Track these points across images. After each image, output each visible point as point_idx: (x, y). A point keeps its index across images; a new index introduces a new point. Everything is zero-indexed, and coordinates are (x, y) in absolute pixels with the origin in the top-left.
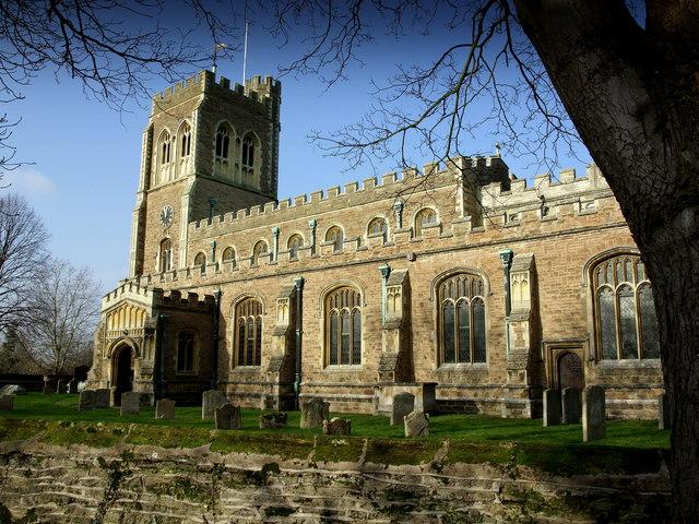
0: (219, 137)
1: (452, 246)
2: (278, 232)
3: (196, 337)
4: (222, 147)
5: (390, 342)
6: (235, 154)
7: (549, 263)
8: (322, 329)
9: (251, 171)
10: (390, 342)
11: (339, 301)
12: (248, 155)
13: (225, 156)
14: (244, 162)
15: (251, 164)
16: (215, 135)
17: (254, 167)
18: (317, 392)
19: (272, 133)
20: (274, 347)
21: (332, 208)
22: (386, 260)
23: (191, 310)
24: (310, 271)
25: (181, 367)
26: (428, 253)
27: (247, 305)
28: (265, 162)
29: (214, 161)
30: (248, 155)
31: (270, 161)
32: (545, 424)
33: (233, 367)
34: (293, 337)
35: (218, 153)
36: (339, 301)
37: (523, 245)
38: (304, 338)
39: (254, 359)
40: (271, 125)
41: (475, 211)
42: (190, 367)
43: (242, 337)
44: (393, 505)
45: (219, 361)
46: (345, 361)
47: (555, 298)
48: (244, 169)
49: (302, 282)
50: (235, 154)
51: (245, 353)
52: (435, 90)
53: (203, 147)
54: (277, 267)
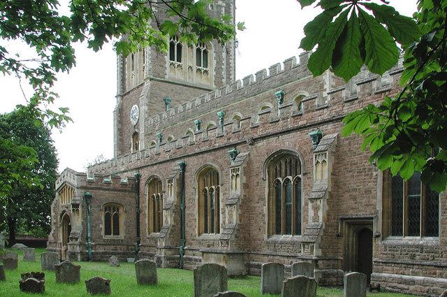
0: (172, 45)
1: (280, 129)
2: (199, 124)
3: (121, 210)
5: (231, 216)
6: (189, 57)
7: (350, 144)
8: (197, 205)
9: (206, 72)
10: (231, 216)
11: (283, 171)
12: (202, 56)
13: (179, 60)
14: (199, 64)
15: (206, 66)
18: (194, 255)
20: (168, 219)
21: (234, 101)
22: (235, 145)
23: (114, 190)
24: (189, 156)
26: (263, 138)
27: (154, 182)
28: (219, 62)
29: (167, 65)
30: (202, 56)
33: (149, 234)
34: (245, 205)
35: (172, 58)
36: (283, 171)
37: (330, 126)
38: (187, 212)
39: (157, 228)
42: (117, 233)
43: (278, 201)
45: (187, 229)
46: (287, 232)
47: (352, 176)
48: (199, 70)
49: (184, 166)
50: (189, 57)
51: (157, 224)
52: (73, 65)
54: (170, 153)
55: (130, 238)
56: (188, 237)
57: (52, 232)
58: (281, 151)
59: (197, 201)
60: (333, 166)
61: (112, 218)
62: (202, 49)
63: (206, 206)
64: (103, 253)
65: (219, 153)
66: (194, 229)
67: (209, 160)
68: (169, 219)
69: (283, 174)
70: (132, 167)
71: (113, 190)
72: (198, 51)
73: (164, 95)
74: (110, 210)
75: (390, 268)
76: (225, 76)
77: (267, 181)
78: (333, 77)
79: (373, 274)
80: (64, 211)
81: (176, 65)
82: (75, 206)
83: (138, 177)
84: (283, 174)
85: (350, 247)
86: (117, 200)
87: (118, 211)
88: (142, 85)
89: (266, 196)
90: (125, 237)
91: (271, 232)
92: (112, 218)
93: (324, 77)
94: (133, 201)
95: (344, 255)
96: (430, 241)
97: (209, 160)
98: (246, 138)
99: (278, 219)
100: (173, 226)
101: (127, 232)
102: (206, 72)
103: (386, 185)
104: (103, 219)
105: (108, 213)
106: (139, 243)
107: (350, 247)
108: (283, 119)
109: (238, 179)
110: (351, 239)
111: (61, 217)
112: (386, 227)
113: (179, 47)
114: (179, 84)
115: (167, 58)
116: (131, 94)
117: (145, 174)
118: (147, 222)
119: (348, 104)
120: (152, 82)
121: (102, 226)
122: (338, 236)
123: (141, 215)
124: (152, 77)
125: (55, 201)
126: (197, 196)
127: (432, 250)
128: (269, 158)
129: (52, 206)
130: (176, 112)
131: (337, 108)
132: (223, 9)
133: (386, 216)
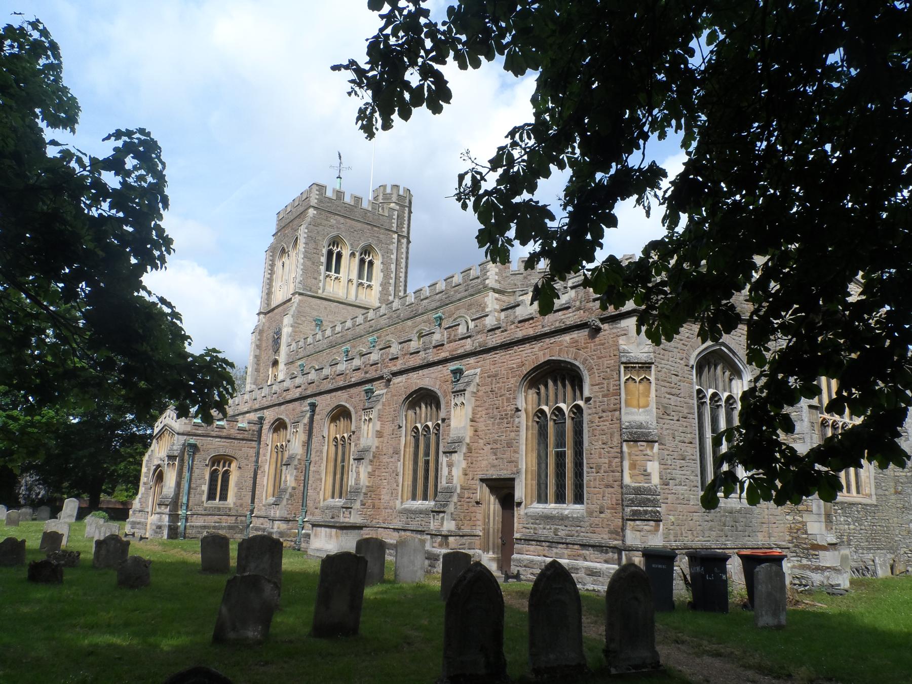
0: (330, 253)
3: (233, 465)
4: (333, 261)
6: (349, 267)
8: (325, 459)
9: (369, 286)
13: (337, 271)
14: (360, 276)
15: (369, 278)
16: (325, 251)
17: (372, 283)
19: (395, 245)
25: (211, 496)
28: (387, 276)
29: (322, 278)
30: (365, 266)
31: (393, 275)
32: (165, 537)
35: (328, 268)
37: (472, 360)
39: (543, 495)
40: (395, 236)
41: (709, 502)
42: (224, 497)
44: (632, 510)
49: (313, 406)
50: (349, 267)
53: (309, 263)
55: (241, 505)
56: (310, 503)
57: (139, 496)
58: (421, 389)
59: (325, 455)
60: (473, 410)
61: (220, 477)
62: (367, 259)
63: (336, 460)
64: (201, 527)
65: (353, 391)
66: (318, 493)
67: (341, 398)
68: (288, 478)
69: (423, 421)
70: (257, 406)
71: (226, 438)
72: (362, 261)
73: (315, 314)
74: (218, 465)
75: (532, 548)
76: (392, 293)
77: (404, 429)
78: (496, 299)
79: (515, 556)
80: (159, 466)
81: (333, 278)
82: (171, 457)
83: (261, 419)
84: (423, 421)
85: (491, 519)
86: (229, 452)
87: (229, 466)
88: (290, 300)
89: (402, 449)
90: (235, 504)
91: (405, 497)
92: (220, 477)
93: (486, 299)
94: (252, 452)
95: (484, 529)
96: (570, 509)
97: (341, 398)
98: (385, 372)
99: (342, 474)
100: (294, 488)
101: (239, 497)
102: (369, 286)
103: (530, 436)
104: (207, 477)
105: (216, 470)
106: (252, 512)
107: (491, 519)
108: (425, 350)
109: (371, 425)
110: (492, 507)
111: (154, 474)
112: (529, 491)
113: (339, 255)
114: (334, 301)
115: (323, 268)
116: (276, 311)
117: (270, 416)
118: (265, 483)
119: (490, 333)
120: (300, 297)
121: (205, 488)
122: (478, 503)
123: (259, 472)
124: (301, 291)
125: (149, 452)
126: (326, 447)
127: (576, 522)
128: (407, 398)
129: (145, 458)
130: (323, 336)
131: (480, 338)
132: (396, 213)
133: (529, 477)
